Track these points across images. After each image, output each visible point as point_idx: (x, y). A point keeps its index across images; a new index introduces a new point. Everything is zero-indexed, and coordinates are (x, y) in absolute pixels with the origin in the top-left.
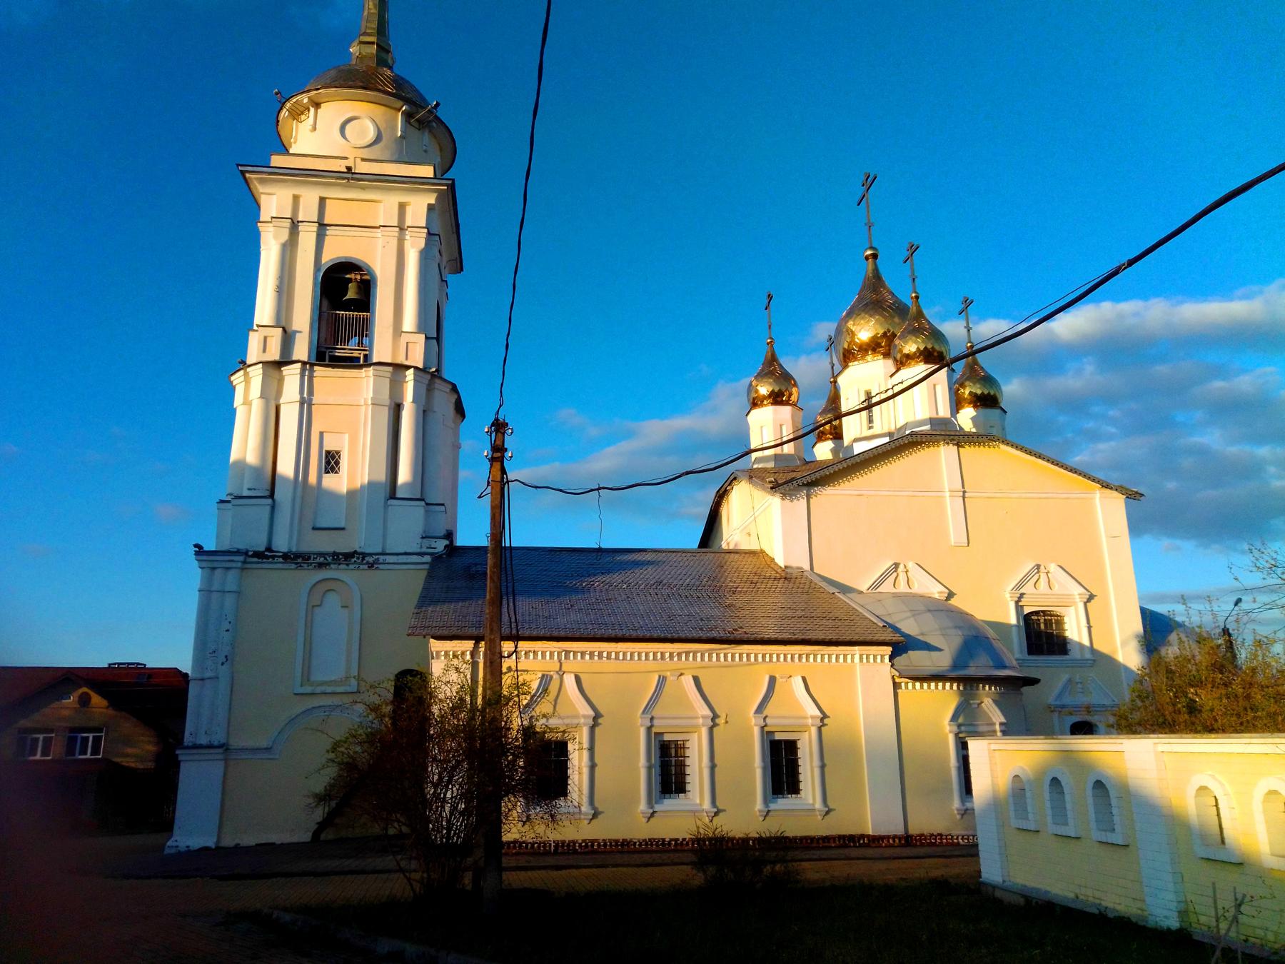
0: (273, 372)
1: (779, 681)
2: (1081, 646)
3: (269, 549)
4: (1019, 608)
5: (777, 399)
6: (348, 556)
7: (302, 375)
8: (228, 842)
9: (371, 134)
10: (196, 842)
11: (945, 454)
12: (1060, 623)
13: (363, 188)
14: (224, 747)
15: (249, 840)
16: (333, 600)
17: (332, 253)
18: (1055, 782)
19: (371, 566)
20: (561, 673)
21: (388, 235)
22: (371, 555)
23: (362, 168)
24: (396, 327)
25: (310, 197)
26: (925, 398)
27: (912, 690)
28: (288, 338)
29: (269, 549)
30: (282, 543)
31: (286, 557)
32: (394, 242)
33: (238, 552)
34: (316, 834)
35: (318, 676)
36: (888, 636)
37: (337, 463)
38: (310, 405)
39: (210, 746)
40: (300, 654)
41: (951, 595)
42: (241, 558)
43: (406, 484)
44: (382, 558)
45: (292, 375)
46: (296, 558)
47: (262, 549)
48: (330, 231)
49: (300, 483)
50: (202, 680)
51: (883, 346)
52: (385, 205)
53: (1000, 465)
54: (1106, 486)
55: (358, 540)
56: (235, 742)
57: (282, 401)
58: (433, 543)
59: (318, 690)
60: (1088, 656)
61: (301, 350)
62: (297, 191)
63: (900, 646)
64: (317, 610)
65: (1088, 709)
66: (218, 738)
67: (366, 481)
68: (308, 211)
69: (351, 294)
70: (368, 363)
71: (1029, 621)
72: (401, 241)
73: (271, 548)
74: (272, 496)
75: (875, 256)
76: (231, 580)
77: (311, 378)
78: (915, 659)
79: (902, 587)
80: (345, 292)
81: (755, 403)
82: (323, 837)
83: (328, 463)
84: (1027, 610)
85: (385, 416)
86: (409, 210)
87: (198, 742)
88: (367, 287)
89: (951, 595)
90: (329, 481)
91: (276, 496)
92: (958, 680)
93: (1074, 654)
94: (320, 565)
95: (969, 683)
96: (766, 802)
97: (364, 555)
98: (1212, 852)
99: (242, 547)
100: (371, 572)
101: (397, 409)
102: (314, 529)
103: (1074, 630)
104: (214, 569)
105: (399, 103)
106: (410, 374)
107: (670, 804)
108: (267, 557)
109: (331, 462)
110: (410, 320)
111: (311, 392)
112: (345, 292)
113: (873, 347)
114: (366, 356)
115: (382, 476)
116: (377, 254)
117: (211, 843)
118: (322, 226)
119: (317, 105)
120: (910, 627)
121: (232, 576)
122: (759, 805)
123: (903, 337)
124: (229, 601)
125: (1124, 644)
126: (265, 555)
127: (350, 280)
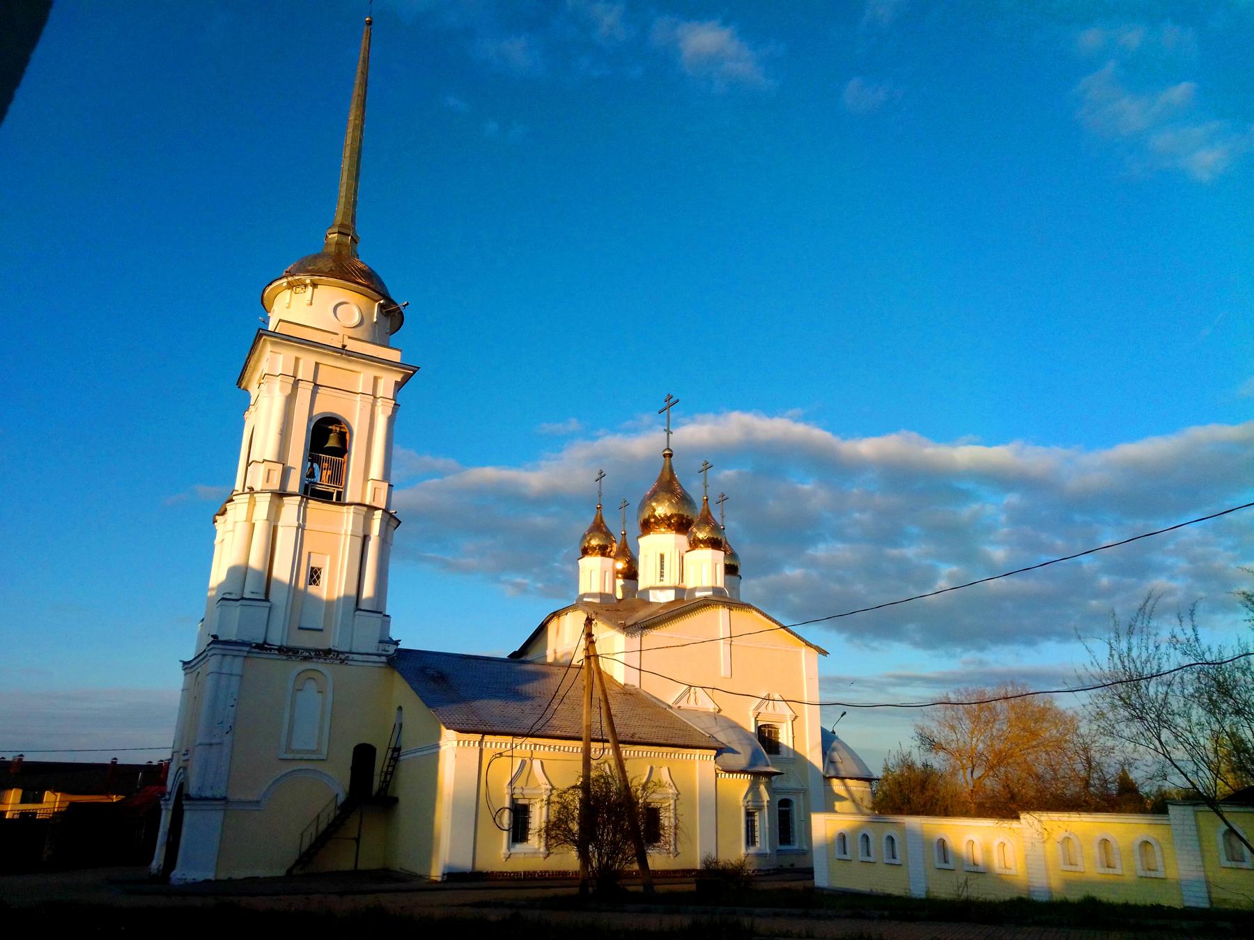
0: (276, 500)
1: (655, 769)
2: (788, 748)
3: (265, 642)
4: (756, 721)
5: (603, 551)
6: (328, 652)
7: (300, 506)
8: (223, 876)
9: (356, 319)
10: (200, 876)
11: (722, 613)
12: (777, 733)
13: (350, 361)
14: (224, 799)
15: (239, 874)
16: (311, 687)
17: (322, 408)
18: (866, 837)
19: (342, 661)
20: (531, 759)
21: (364, 401)
22: (343, 653)
23: (352, 346)
24: (365, 473)
25: (308, 361)
26: (704, 569)
27: (724, 777)
28: (286, 473)
29: (265, 642)
30: (276, 639)
31: (281, 650)
32: (369, 407)
33: (243, 644)
34: (289, 871)
35: (296, 745)
36: (715, 745)
37: (318, 577)
38: (303, 529)
39: (214, 799)
40: (286, 727)
41: (720, 711)
42: (247, 649)
43: (368, 599)
44: (351, 656)
45: (291, 507)
46: (288, 652)
47: (261, 642)
48: (321, 390)
49: (292, 588)
50: (211, 745)
51: (682, 525)
52: (363, 377)
53: (748, 620)
54: (808, 644)
55: (334, 641)
56: (231, 798)
57: (280, 524)
58: (386, 647)
59: (298, 756)
60: (791, 756)
61: (294, 485)
62: (299, 354)
63: (720, 750)
64: (299, 694)
65: (788, 791)
66: (219, 793)
67: (342, 594)
68: (305, 372)
69: (332, 442)
70: (340, 501)
71: (760, 729)
72: (373, 406)
73: (259, 639)
74: (267, 599)
75: (671, 455)
76: (236, 665)
77: (305, 508)
78: (726, 756)
79: (692, 705)
80: (327, 439)
81: (585, 552)
82: (294, 872)
83: (312, 576)
84: (760, 724)
85: (359, 542)
86: (381, 383)
87: (203, 795)
88: (344, 440)
89: (720, 711)
90: (312, 589)
91: (271, 598)
92: (751, 773)
93: (784, 754)
94: (305, 658)
95: (756, 775)
96: (509, 848)
97: (339, 653)
98: (979, 872)
99: (246, 639)
100: (343, 667)
101: (366, 538)
102: (300, 628)
103: (785, 738)
104: (224, 655)
105: (376, 296)
106: (378, 514)
107: (519, 847)
108: (266, 649)
109: (314, 576)
110: (376, 470)
111: (304, 520)
112: (327, 439)
113: (667, 522)
114: (339, 494)
115: (353, 592)
116: (355, 415)
117: (211, 876)
118: (316, 386)
119: (314, 285)
120: (723, 738)
121: (239, 661)
122: (504, 849)
123: (698, 526)
124: (235, 680)
125: (811, 749)
126: (263, 647)
127: (331, 431)
